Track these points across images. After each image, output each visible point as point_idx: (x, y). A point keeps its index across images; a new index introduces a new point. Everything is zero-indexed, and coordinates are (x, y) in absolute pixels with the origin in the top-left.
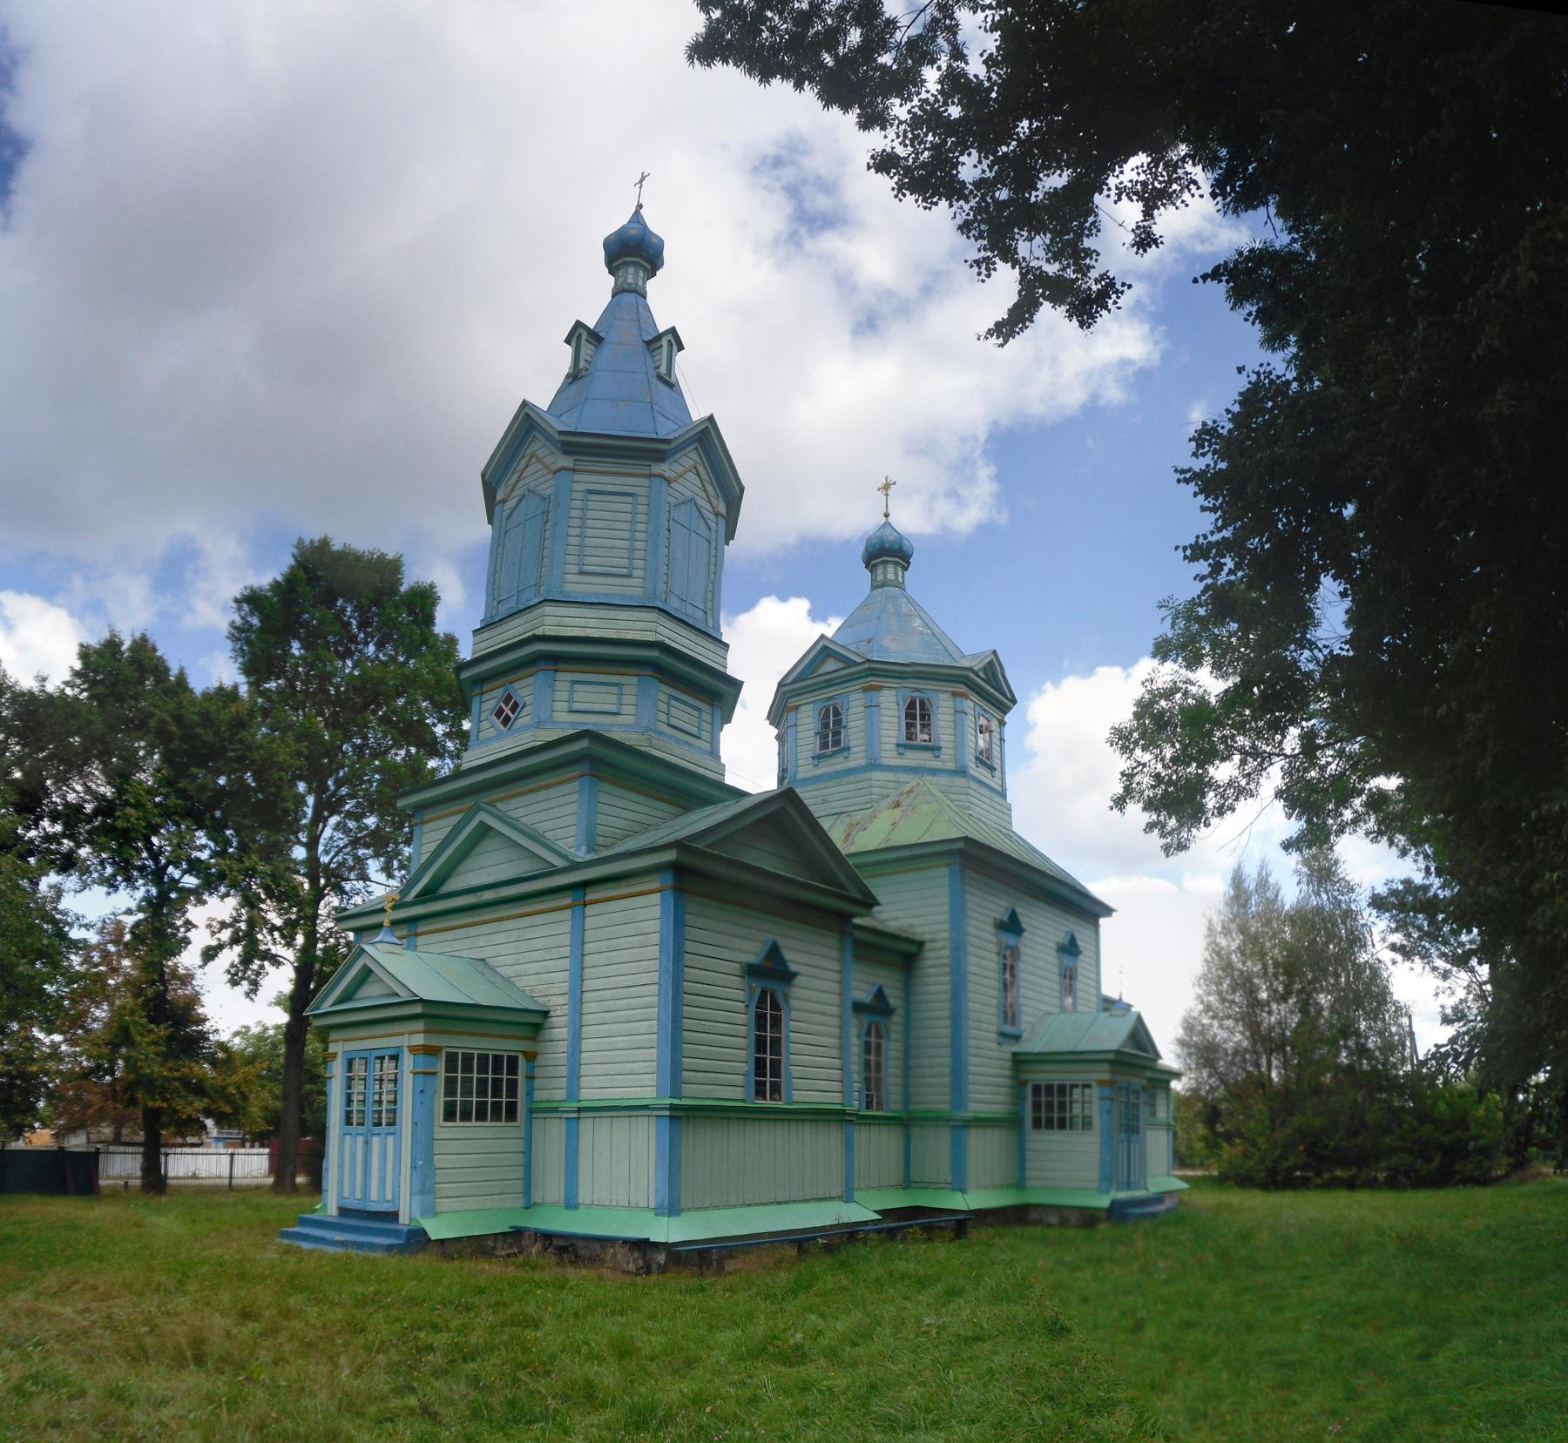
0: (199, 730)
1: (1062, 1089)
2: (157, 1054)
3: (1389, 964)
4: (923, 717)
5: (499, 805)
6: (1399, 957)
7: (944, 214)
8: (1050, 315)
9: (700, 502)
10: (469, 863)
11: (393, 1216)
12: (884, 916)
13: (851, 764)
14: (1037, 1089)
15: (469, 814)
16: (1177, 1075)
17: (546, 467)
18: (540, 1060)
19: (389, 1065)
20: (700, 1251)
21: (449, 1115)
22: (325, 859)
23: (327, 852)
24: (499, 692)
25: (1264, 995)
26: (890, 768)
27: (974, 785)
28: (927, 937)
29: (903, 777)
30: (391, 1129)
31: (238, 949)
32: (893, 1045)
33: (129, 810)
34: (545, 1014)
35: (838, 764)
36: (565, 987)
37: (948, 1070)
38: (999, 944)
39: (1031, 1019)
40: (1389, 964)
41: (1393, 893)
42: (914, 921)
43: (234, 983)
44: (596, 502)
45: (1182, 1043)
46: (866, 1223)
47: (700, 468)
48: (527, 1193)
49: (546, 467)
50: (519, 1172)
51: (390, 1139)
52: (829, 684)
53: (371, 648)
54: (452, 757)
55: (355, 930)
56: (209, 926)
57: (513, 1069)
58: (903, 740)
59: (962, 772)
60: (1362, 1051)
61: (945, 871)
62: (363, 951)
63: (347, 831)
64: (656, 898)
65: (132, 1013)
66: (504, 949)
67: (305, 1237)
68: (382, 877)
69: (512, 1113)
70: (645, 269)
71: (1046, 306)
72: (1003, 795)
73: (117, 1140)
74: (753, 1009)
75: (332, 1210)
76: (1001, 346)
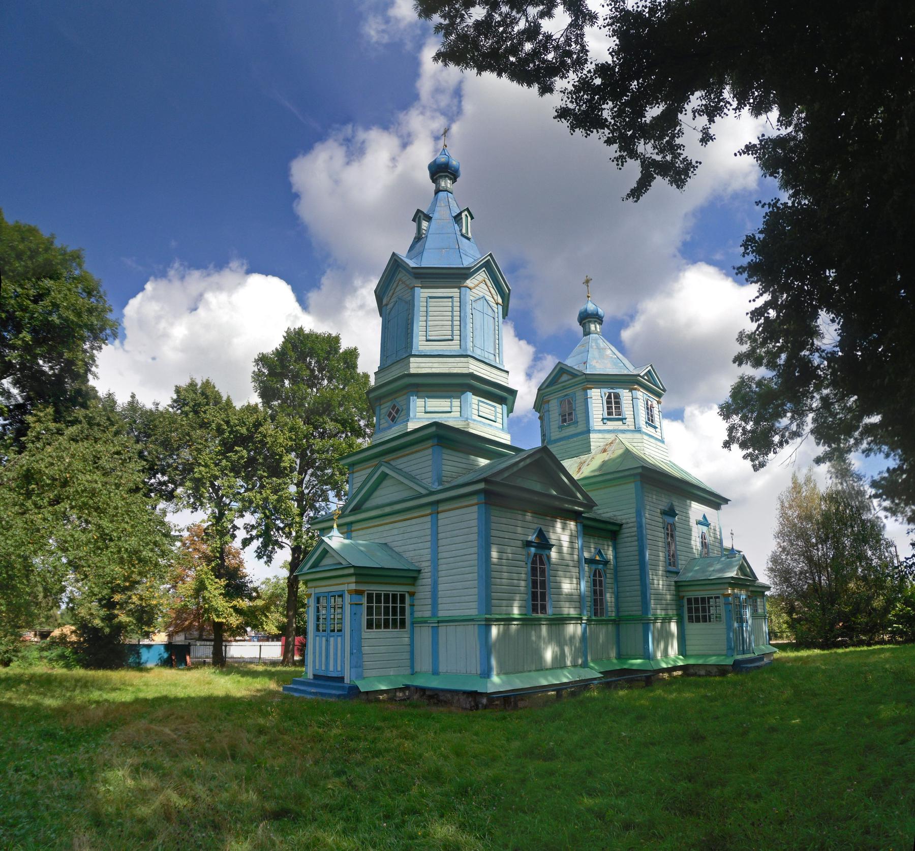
0: (238, 428)
1: (703, 599)
2: (221, 594)
3: (883, 518)
4: (616, 403)
5: (392, 462)
6: (889, 514)
7: (598, 137)
8: (660, 183)
9: (488, 298)
10: (376, 494)
11: (342, 679)
12: (599, 512)
13: (579, 431)
14: (689, 600)
15: (377, 467)
16: (768, 588)
17: (407, 286)
18: (417, 596)
19: (339, 600)
20: (504, 697)
21: (370, 625)
22: (306, 491)
23: (307, 488)
24: (389, 404)
25: (814, 540)
26: (600, 431)
27: (646, 437)
28: (624, 521)
29: (607, 436)
30: (340, 633)
31: (261, 540)
32: (608, 581)
33: (202, 468)
34: (419, 571)
35: (571, 430)
36: (429, 557)
37: (639, 593)
38: (664, 522)
39: (684, 562)
40: (883, 518)
41: (884, 479)
42: (617, 513)
43: (259, 557)
44: (432, 302)
45: (771, 570)
46: (595, 679)
47: (487, 281)
48: (412, 666)
49: (407, 286)
50: (407, 656)
51: (339, 639)
52: (564, 388)
53: (326, 382)
54: (369, 437)
55: (320, 530)
56: (245, 528)
57: (403, 600)
58: (606, 416)
59: (638, 430)
60: (869, 567)
61: (633, 485)
62: (323, 541)
63: (317, 476)
64: (475, 508)
65: (206, 573)
66: (396, 538)
67: (296, 690)
68: (336, 500)
69: (403, 624)
70: (450, 179)
71: (659, 178)
72: (662, 441)
73: (200, 639)
74: (529, 565)
75: (310, 676)
76: (636, 201)
